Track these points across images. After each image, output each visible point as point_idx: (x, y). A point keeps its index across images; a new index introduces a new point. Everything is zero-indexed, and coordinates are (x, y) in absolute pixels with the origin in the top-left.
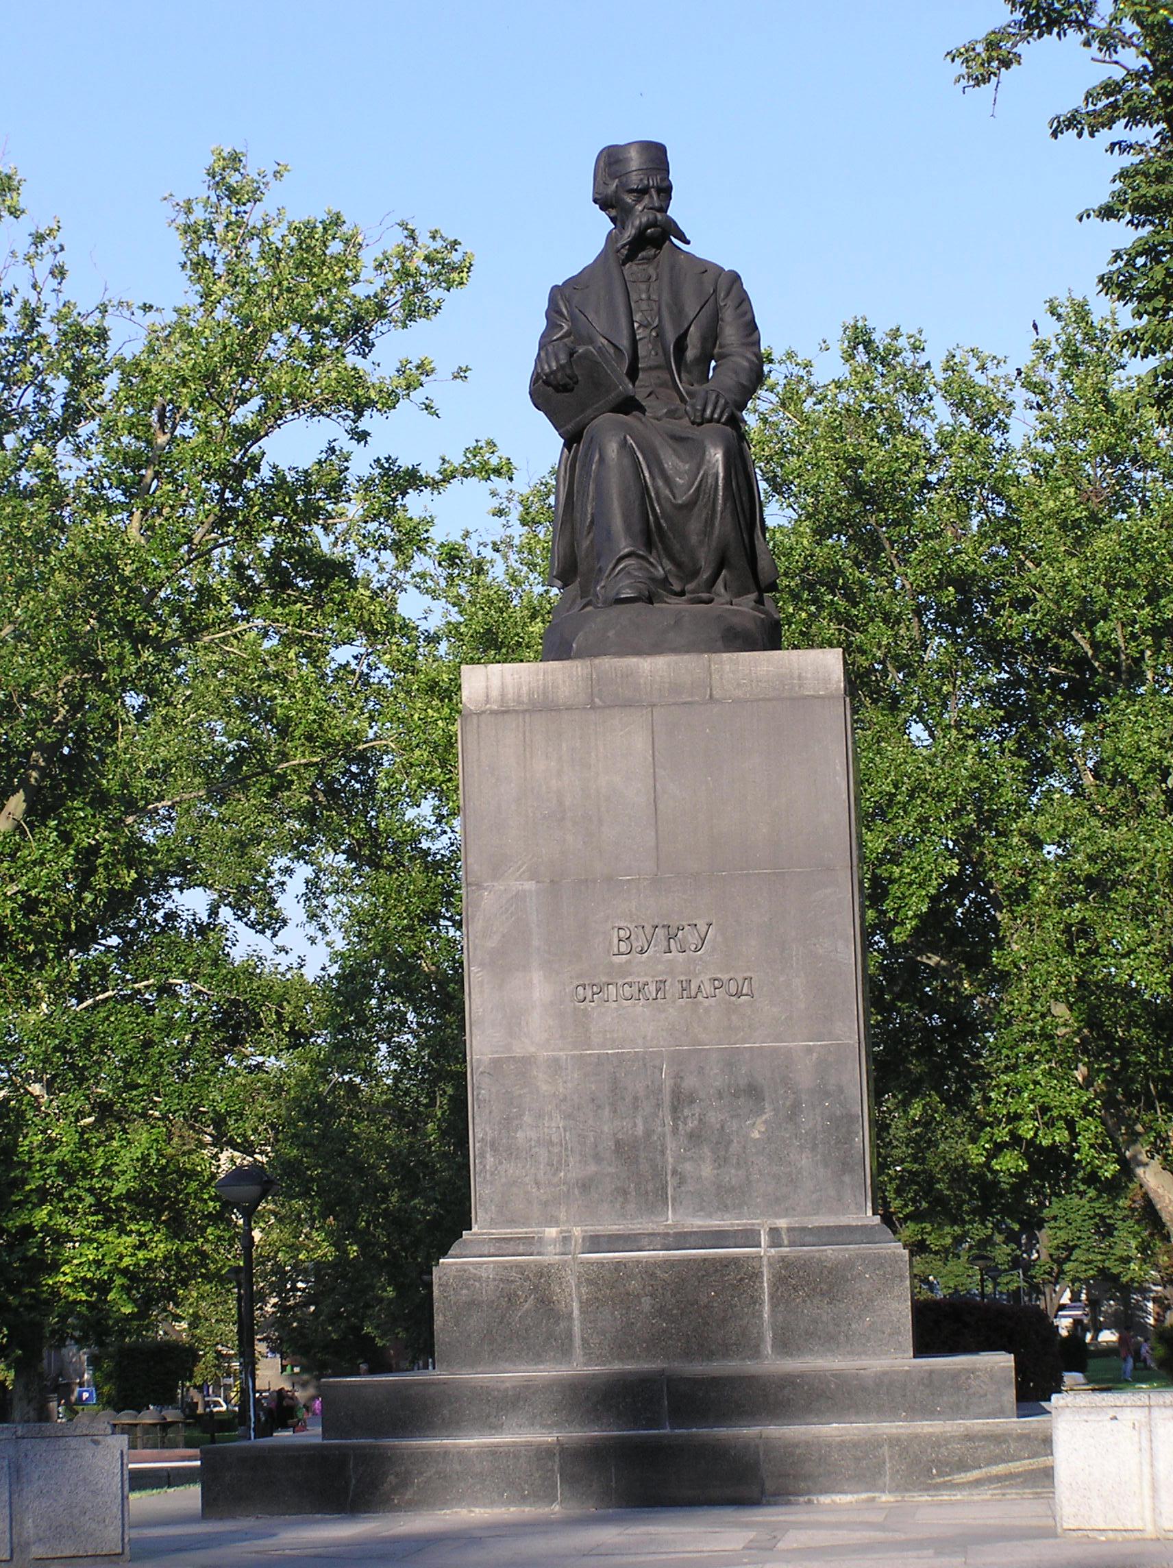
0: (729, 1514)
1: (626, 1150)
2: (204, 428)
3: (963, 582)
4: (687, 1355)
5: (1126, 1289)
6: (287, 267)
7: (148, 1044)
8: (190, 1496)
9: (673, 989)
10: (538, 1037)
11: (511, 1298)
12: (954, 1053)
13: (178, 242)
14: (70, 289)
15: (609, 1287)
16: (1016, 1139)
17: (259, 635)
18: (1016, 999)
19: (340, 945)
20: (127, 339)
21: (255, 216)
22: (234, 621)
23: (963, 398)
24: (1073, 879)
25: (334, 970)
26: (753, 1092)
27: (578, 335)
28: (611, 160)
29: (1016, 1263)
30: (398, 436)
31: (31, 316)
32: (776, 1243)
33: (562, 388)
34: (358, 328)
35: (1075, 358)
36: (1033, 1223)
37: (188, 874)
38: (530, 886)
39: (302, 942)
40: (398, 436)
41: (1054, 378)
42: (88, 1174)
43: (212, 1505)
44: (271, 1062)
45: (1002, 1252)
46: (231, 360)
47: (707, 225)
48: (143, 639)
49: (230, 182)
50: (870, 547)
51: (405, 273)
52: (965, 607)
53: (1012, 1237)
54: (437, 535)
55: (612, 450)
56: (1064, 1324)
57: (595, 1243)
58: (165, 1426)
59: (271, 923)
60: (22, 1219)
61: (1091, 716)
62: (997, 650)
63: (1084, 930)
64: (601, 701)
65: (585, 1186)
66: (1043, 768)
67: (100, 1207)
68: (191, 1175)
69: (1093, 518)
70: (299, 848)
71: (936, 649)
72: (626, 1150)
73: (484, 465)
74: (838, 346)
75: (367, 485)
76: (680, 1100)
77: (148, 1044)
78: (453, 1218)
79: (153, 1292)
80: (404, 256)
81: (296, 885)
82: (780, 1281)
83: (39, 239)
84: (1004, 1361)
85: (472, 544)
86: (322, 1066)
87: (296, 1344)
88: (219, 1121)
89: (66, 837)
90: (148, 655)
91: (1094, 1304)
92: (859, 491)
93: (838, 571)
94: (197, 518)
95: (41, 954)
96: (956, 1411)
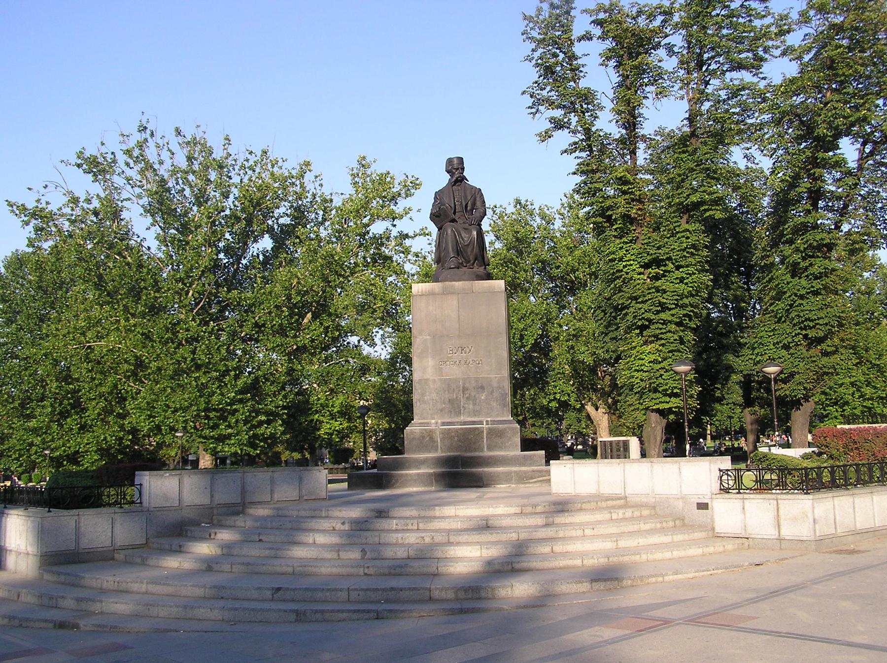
0: (475, 489)
1: (451, 401)
2: (356, 223)
3: (543, 262)
4: (466, 451)
5: (584, 435)
6: (376, 184)
7: (343, 374)
8: (345, 485)
9: (463, 362)
10: (430, 374)
11: (423, 437)
12: (541, 378)
13: (350, 178)
14: (324, 190)
15: (447, 434)
16: (555, 399)
17: (369, 274)
18: (555, 365)
19: (390, 351)
20: (337, 202)
21: (369, 172)
22: (363, 271)
23: (543, 218)
24: (570, 335)
25: (388, 357)
26: (482, 388)
27: (442, 204)
28: (450, 161)
29: (557, 429)
30: (403, 226)
31: (314, 196)
32: (487, 424)
33: (437, 216)
34: (394, 199)
35: (571, 207)
36: (561, 419)
37: (353, 333)
38: (428, 337)
39: (380, 350)
40: (403, 226)
41: (566, 212)
42: (328, 407)
43: (350, 487)
44: (373, 379)
45: (553, 426)
46: (363, 207)
47: (473, 178)
48: (341, 275)
49: (363, 163)
50: (521, 253)
51: (405, 186)
52: (544, 268)
53: (556, 423)
54: (413, 250)
55: (449, 231)
56: (569, 444)
57: (443, 424)
58: (346, 468)
59: (373, 345)
60: (311, 418)
61: (574, 295)
62: (552, 279)
63: (572, 347)
64: (445, 292)
65: (441, 410)
66: (564, 307)
67: (331, 415)
68: (354, 407)
69: (575, 246)
70: (379, 326)
71: (537, 278)
72: (451, 401)
73: (424, 233)
74: (512, 205)
75: (396, 237)
76: (465, 389)
77: (343, 374)
78: (408, 420)
79: (344, 435)
80: (405, 181)
81: (379, 336)
82: (488, 434)
83: (316, 177)
84: (543, 452)
85: (423, 252)
86: (385, 380)
87: (379, 448)
88: (360, 394)
89: (321, 324)
90: (341, 279)
91: (576, 439)
92: (517, 239)
93: (513, 259)
94: (353, 245)
95: (315, 352)
96: (530, 465)
